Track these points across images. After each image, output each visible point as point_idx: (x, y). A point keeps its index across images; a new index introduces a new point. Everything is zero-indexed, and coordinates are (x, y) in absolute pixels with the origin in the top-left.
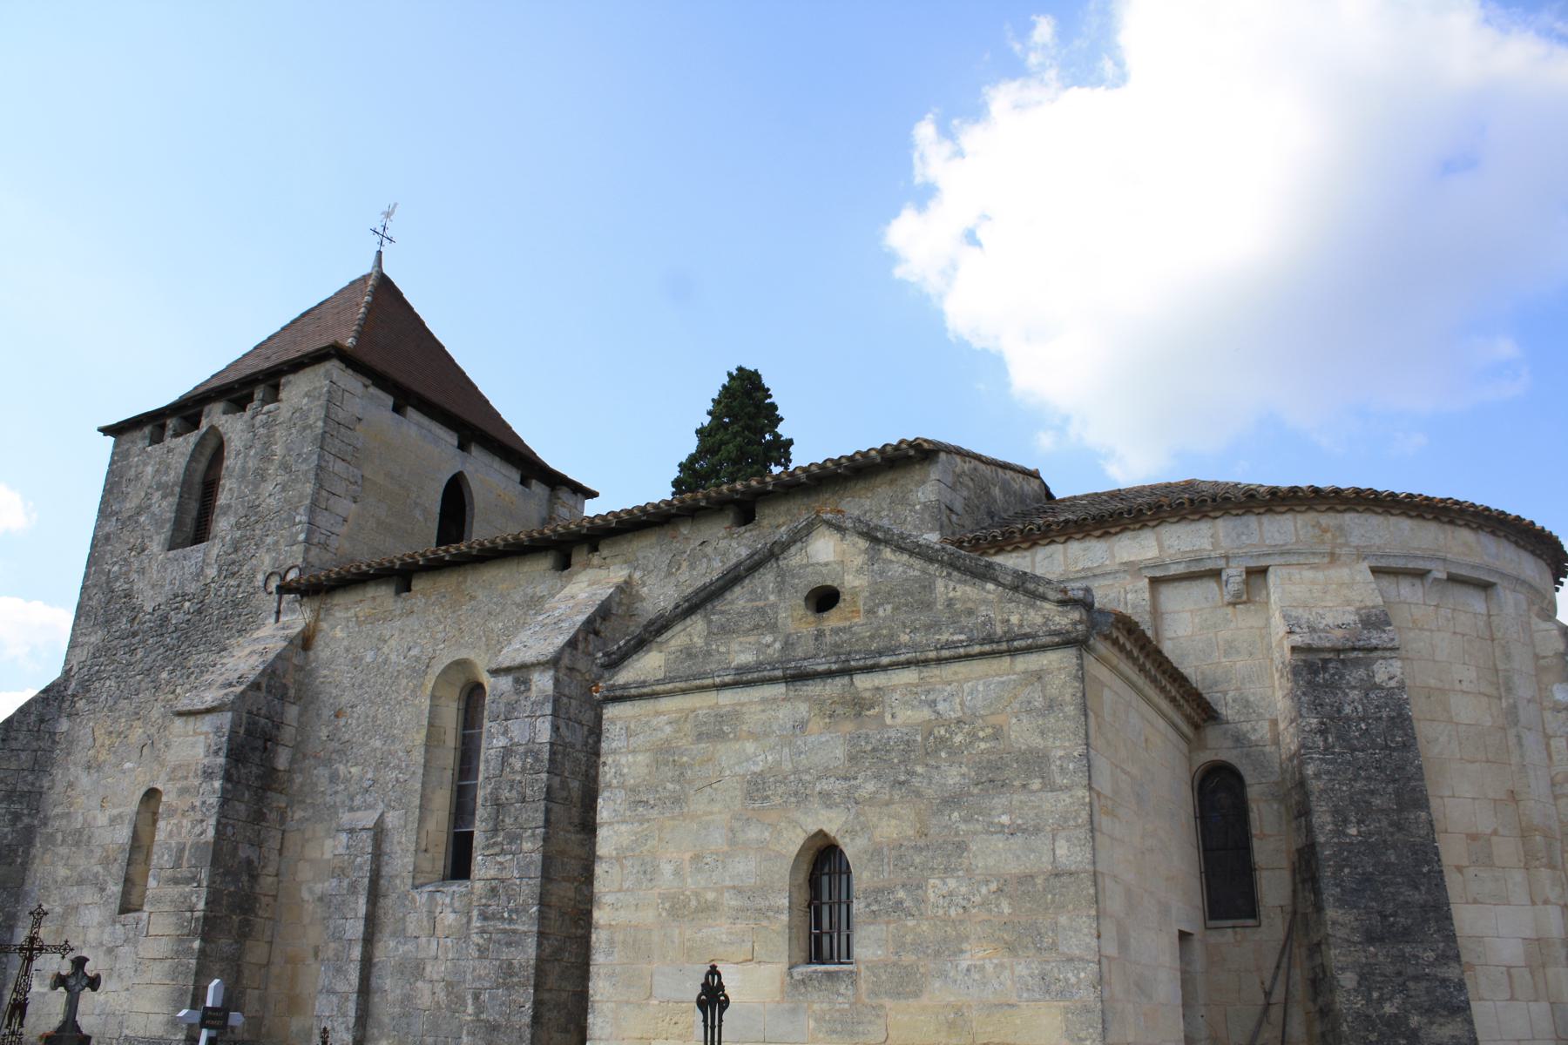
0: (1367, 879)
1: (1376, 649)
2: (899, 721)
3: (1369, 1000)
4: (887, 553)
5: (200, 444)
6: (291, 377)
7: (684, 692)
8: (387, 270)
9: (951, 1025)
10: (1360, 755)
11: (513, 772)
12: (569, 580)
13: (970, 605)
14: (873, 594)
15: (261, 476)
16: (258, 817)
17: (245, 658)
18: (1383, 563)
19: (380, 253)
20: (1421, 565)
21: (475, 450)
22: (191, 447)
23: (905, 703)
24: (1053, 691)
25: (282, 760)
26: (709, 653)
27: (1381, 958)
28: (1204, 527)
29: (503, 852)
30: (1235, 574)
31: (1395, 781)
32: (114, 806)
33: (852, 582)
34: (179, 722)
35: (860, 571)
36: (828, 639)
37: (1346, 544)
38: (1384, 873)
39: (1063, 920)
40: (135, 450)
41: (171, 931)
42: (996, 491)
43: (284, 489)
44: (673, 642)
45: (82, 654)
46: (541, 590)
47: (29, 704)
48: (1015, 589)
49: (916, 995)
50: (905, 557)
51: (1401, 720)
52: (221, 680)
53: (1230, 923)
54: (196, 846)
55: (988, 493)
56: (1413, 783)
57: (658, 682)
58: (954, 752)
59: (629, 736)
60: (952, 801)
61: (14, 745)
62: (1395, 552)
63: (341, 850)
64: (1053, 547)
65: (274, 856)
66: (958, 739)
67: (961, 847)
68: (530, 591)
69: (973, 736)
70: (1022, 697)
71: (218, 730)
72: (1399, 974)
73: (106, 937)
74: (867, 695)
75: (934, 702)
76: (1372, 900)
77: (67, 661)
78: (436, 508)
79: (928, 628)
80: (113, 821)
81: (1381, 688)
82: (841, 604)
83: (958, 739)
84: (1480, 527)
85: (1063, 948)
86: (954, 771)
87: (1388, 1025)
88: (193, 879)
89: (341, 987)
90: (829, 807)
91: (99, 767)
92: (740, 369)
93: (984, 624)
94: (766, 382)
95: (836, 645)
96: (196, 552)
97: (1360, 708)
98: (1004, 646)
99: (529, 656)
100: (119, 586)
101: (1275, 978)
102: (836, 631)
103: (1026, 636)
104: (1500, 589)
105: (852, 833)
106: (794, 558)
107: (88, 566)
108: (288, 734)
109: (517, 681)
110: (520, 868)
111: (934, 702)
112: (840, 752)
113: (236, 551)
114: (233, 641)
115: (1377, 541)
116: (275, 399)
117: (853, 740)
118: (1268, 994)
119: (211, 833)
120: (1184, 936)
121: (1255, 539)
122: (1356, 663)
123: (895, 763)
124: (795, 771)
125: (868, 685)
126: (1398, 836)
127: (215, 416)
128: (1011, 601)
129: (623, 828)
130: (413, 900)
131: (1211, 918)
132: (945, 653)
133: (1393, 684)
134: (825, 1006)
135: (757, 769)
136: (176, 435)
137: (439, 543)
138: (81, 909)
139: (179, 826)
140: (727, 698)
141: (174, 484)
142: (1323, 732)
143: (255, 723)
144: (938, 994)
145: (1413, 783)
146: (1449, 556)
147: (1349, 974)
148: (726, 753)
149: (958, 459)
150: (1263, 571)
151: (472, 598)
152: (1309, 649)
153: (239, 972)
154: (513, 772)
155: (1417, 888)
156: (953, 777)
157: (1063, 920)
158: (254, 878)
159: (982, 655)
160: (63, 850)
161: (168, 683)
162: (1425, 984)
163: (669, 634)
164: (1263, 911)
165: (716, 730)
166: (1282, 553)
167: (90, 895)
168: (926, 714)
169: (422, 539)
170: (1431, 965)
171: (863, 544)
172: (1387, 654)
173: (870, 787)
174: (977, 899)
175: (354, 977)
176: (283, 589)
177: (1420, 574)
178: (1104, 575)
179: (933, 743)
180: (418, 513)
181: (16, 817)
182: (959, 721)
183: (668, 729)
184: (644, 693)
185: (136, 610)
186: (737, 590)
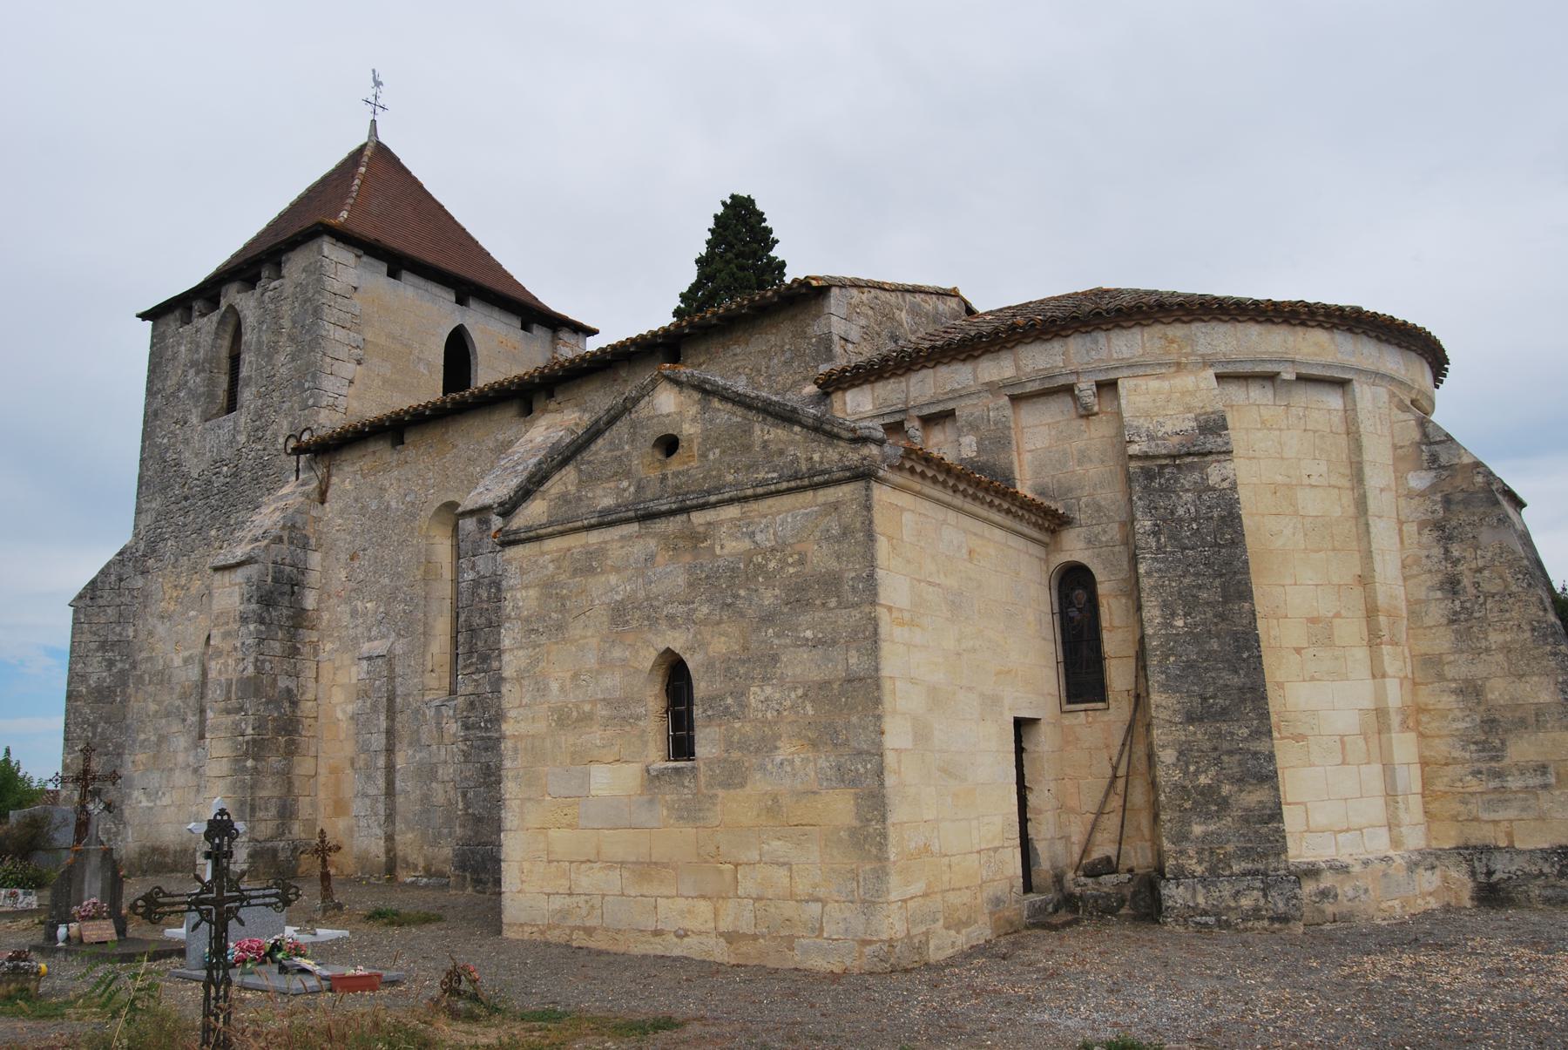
0: (1190, 665)
1: (1210, 453)
2: (726, 551)
3: (1186, 773)
4: (716, 403)
5: (222, 322)
6: (292, 255)
7: (562, 533)
8: (382, 139)
9: (769, 810)
10: (1190, 553)
11: (481, 601)
12: (532, 423)
13: (781, 446)
14: (706, 439)
15: (274, 349)
16: (294, 652)
17: (268, 517)
18: (1230, 369)
19: (374, 122)
20: (1269, 368)
21: (473, 303)
22: (215, 325)
23: (732, 535)
24: (846, 520)
25: (310, 601)
26: (580, 499)
27: (1199, 736)
28: (1056, 346)
29: (478, 671)
31: (1221, 576)
32: (186, 649)
33: (689, 430)
34: (218, 576)
35: (694, 420)
36: (670, 482)
37: (1193, 353)
38: (1206, 660)
39: (854, 719)
40: (170, 331)
41: (228, 753)
42: (903, 316)
44: (552, 491)
45: (148, 519)
46: (509, 434)
47: (108, 566)
48: (816, 429)
49: (742, 785)
50: (730, 406)
51: (1231, 518)
53: (1083, 706)
54: (240, 680)
55: (892, 319)
56: (1239, 577)
57: (541, 526)
58: (769, 577)
59: (522, 574)
60: (768, 619)
61: (101, 602)
62: (1241, 357)
63: (363, 675)
64: (924, 372)
65: (311, 684)
66: (772, 565)
67: (775, 659)
68: (500, 437)
69: (783, 561)
70: (822, 527)
71: (249, 579)
72: (1215, 749)
74: (701, 529)
75: (753, 533)
76: (1194, 684)
77: (136, 526)
78: (440, 361)
79: (748, 468)
80: (186, 661)
81: (1214, 489)
82: (680, 450)
83: (772, 565)
84: (1334, 326)
85: (854, 744)
86: (769, 594)
87: (1202, 794)
88: (242, 708)
89: (372, 791)
90: (673, 628)
91: (170, 617)
92: (733, 197)
93: (792, 462)
94: (759, 207)
95: (677, 487)
96: (227, 421)
97: (1193, 510)
98: (806, 482)
99: (488, 499)
100: (170, 455)
101: (1121, 755)
102: (676, 475)
103: (823, 472)
104: (1356, 385)
105: (691, 649)
106: (643, 410)
107: (143, 441)
108: (313, 578)
109: (480, 522)
110: (490, 683)
111: (753, 533)
112: (681, 580)
114: (265, 499)
115: (1223, 348)
116: (280, 276)
117: (690, 570)
118: (1115, 768)
119: (251, 670)
120: (1022, 726)
121: (1104, 354)
122: (1191, 467)
123: (722, 587)
124: (648, 598)
125: (702, 521)
127: (233, 296)
128: (813, 441)
129: (521, 653)
130: (424, 714)
131: (1069, 702)
132: (760, 490)
133: (1225, 485)
134: (675, 797)
135: (619, 598)
136: (203, 315)
137: (445, 393)
138: (1444, 621)
139: (226, 665)
140: (594, 538)
143: (281, 572)
144: (759, 785)
145: (1239, 577)
146: (1298, 358)
147: (1169, 751)
148: (596, 585)
149: (855, 292)
150: (1113, 384)
151: (454, 446)
153: (290, 783)
154: (481, 601)
155: (1236, 672)
156: (769, 597)
157: (854, 719)
158: (294, 704)
159: (789, 491)
160: (151, 689)
161: (217, 538)
162: (1237, 757)
163: (549, 483)
164: (1111, 695)
165: (588, 565)
166: (1130, 366)
167: (176, 727)
168: (746, 544)
169: (429, 388)
170: (1245, 740)
171: (697, 396)
172: (1222, 457)
173: (705, 610)
174: (788, 703)
175: (381, 783)
176: (297, 451)
177: (1271, 378)
178: (968, 395)
179: (748, 571)
180: (422, 368)
181: (111, 663)
182: (773, 550)
183: (551, 567)
184: (534, 537)
186: (600, 441)
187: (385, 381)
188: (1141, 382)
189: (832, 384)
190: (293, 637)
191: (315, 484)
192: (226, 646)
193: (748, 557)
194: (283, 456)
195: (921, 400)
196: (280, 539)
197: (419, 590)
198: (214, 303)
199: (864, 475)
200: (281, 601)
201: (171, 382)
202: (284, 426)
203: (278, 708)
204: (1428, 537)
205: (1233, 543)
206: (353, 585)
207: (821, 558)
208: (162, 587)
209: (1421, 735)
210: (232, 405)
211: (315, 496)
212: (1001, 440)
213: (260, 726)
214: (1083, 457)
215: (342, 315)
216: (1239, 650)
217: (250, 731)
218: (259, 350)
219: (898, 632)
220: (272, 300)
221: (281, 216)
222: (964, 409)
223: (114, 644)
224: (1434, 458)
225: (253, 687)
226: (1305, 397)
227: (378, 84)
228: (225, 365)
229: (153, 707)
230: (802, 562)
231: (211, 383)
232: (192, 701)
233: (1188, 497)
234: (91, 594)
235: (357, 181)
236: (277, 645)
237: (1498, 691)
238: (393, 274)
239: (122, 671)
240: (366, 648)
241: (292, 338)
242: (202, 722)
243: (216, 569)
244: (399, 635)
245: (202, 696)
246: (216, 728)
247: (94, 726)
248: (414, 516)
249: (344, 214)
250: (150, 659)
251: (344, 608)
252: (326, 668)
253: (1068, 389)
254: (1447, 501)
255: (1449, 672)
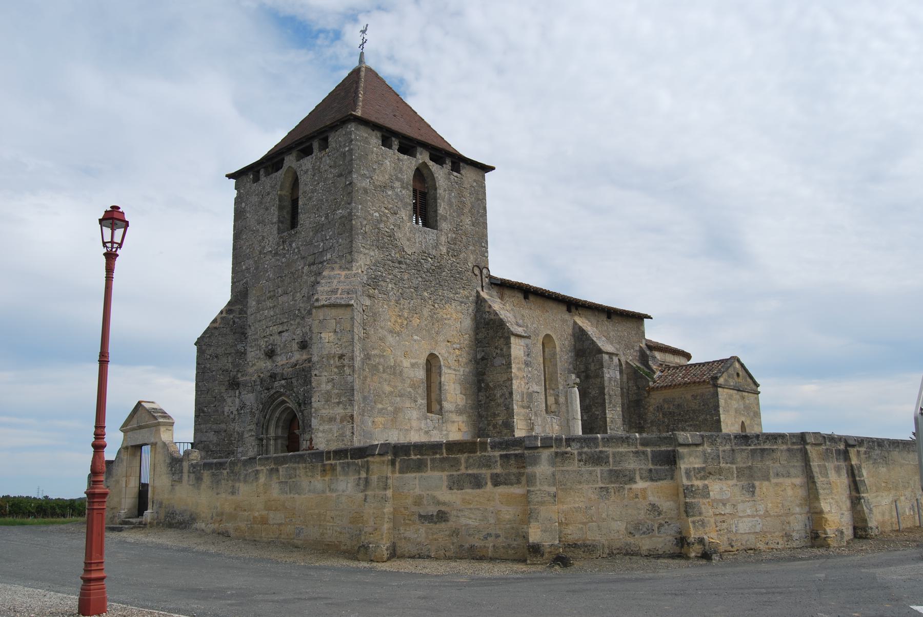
73: (423, 426)
160: (385, 376)
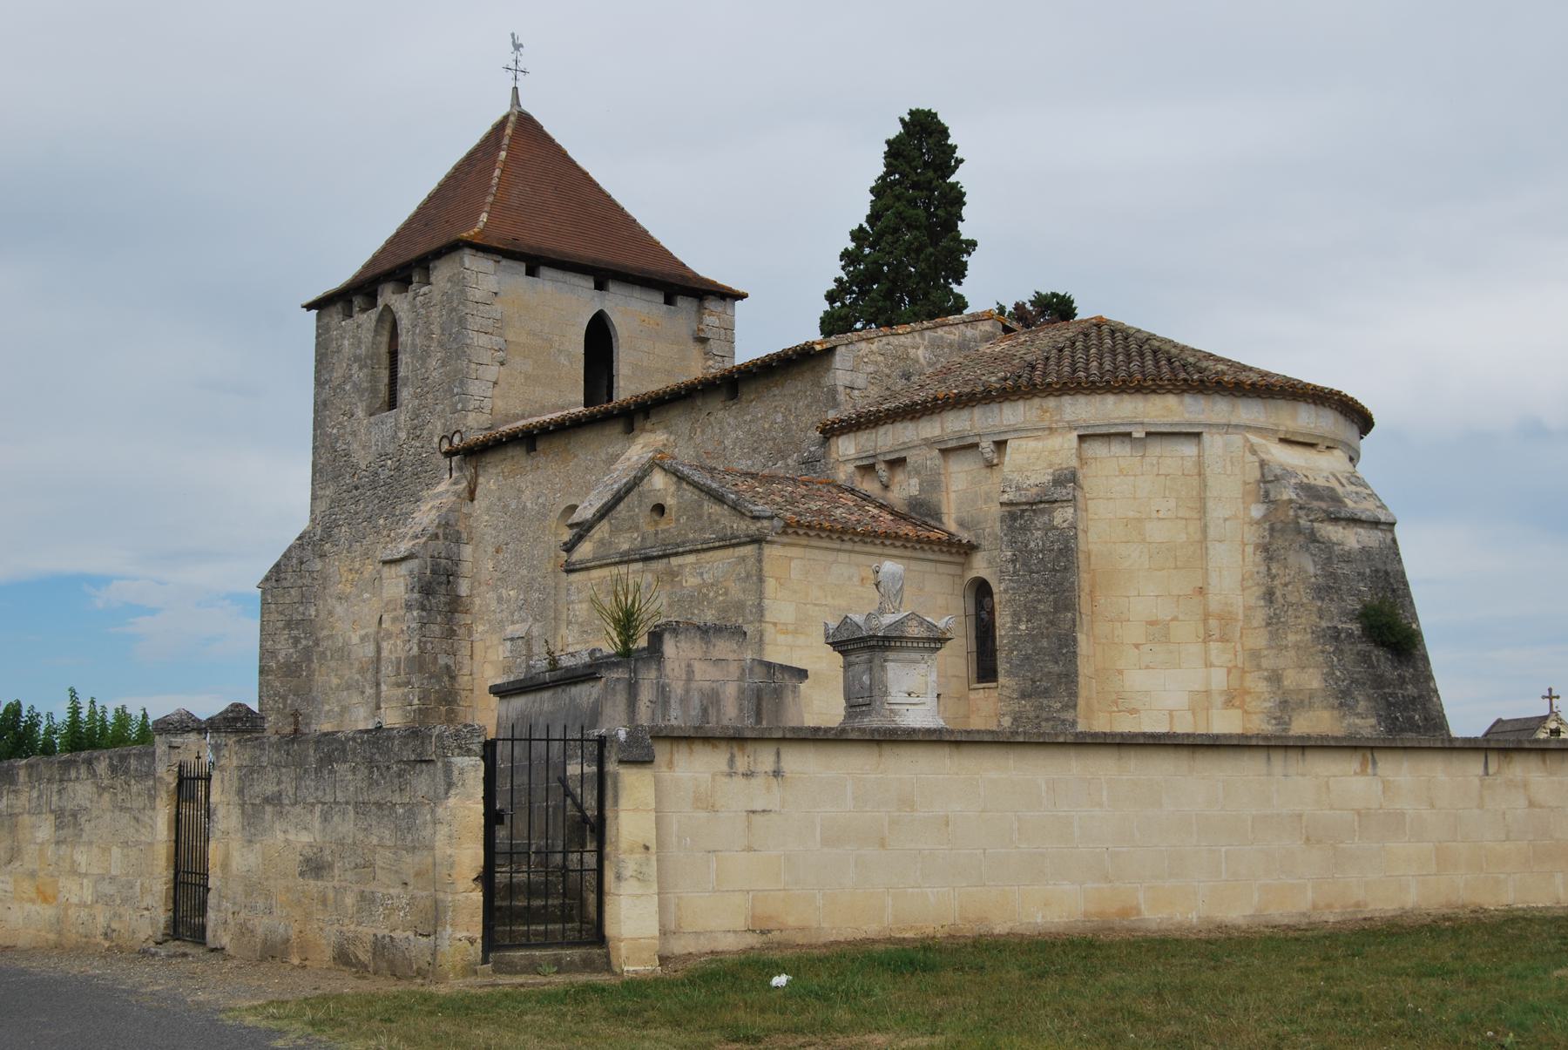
0: (1027, 657)
4: (684, 485)
5: (380, 319)
6: (437, 263)
7: (601, 566)
8: (527, 106)
15: (425, 355)
16: (451, 633)
17: (425, 515)
19: (515, 89)
20: (1122, 429)
21: (612, 287)
25: (464, 588)
28: (965, 414)
30: (986, 445)
32: (363, 628)
33: (670, 502)
43: (443, 365)
45: (323, 505)
46: (617, 448)
47: (289, 550)
52: (411, 533)
61: (285, 584)
65: (467, 661)
71: (411, 572)
77: (312, 512)
80: (363, 639)
92: (912, 113)
100: (340, 446)
102: (663, 531)
108: (466, 568)
113: (418, 416)
119: (415, 650)
122: (1043, 511)
126: (1052, 629)
127: (388, 296)
136: (363, 310)
139: (395, 645)
141: (367, 357)
142: (1013, 561)
150: (1005, 442)
152: (1011, 504)
158: (453, 678)
160: (333, 664)
161: (385, 527)
167: (356, 699)
168: (698, 580)
176: (449, 454)
180: (562, 359)
181: (296, 641)
185: (355, 467)
187: (527, 377)
188: (1023, 442)
189: (830, 432)
190: (451, 620)
191: (465, 484)
192: (395, 629)
193: (699, 588)
194: (439, 455)
195: (885, 449)
196: (436, 536)
197: (550, 582)
198: (371, 300)
199: (758, 540)
200: (439, 590)
201: (337, 375)
202: (438, 427)
203: (439, 681)
204: (1259, 557)
205: (1066, 569)
206: (499, 574)
207: (736, 591)
208: (340, 570)
209: (1246, 712)
210: (392, 403)
211: (466, 494)
212: (933, 483)
213: (424, 698)
214: (988, 498)
215: (485, 322)
216: (1060, 648)
217: (416, 701)
218: (414, 352)
219: (781, 638)
220: (423, 306)
221: (431, 198)
222: (913, 458)
223: (298, 623)
224: (1267, 494)
225: (419, 664)
226: (1156, 449)
227: (517, 47)
228: (385, 360)
229: (335, 681)
230: (726, 594)
231: (374, 378)
232: (369, 675)
233: (1038, 534)
234: (276, 575)
235: (497, 172)
236: (436, 628)
237: (1291, 679)
238: (531, 272)
239: (306, 648)
240: (511, 630)
241: (441, 345)
242: (378, 694)
243: (385, 563)
244: (536, 620)
245: (378, 671)
246: (388, 700)
247: (284, 698)
248: (545, 516)
249: (484, 217)
250: (331, 637)
251: (491, 595)
252: (478, 646)
253: (974, 446)
254: (1272, 529)
255: (1265, 663)
